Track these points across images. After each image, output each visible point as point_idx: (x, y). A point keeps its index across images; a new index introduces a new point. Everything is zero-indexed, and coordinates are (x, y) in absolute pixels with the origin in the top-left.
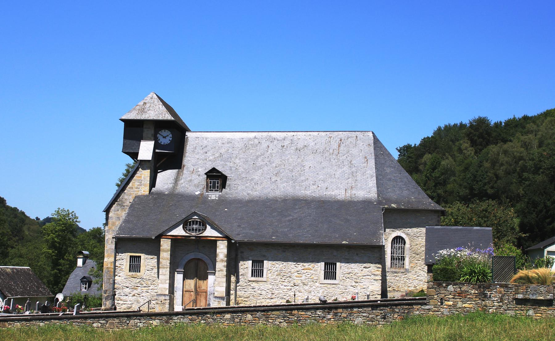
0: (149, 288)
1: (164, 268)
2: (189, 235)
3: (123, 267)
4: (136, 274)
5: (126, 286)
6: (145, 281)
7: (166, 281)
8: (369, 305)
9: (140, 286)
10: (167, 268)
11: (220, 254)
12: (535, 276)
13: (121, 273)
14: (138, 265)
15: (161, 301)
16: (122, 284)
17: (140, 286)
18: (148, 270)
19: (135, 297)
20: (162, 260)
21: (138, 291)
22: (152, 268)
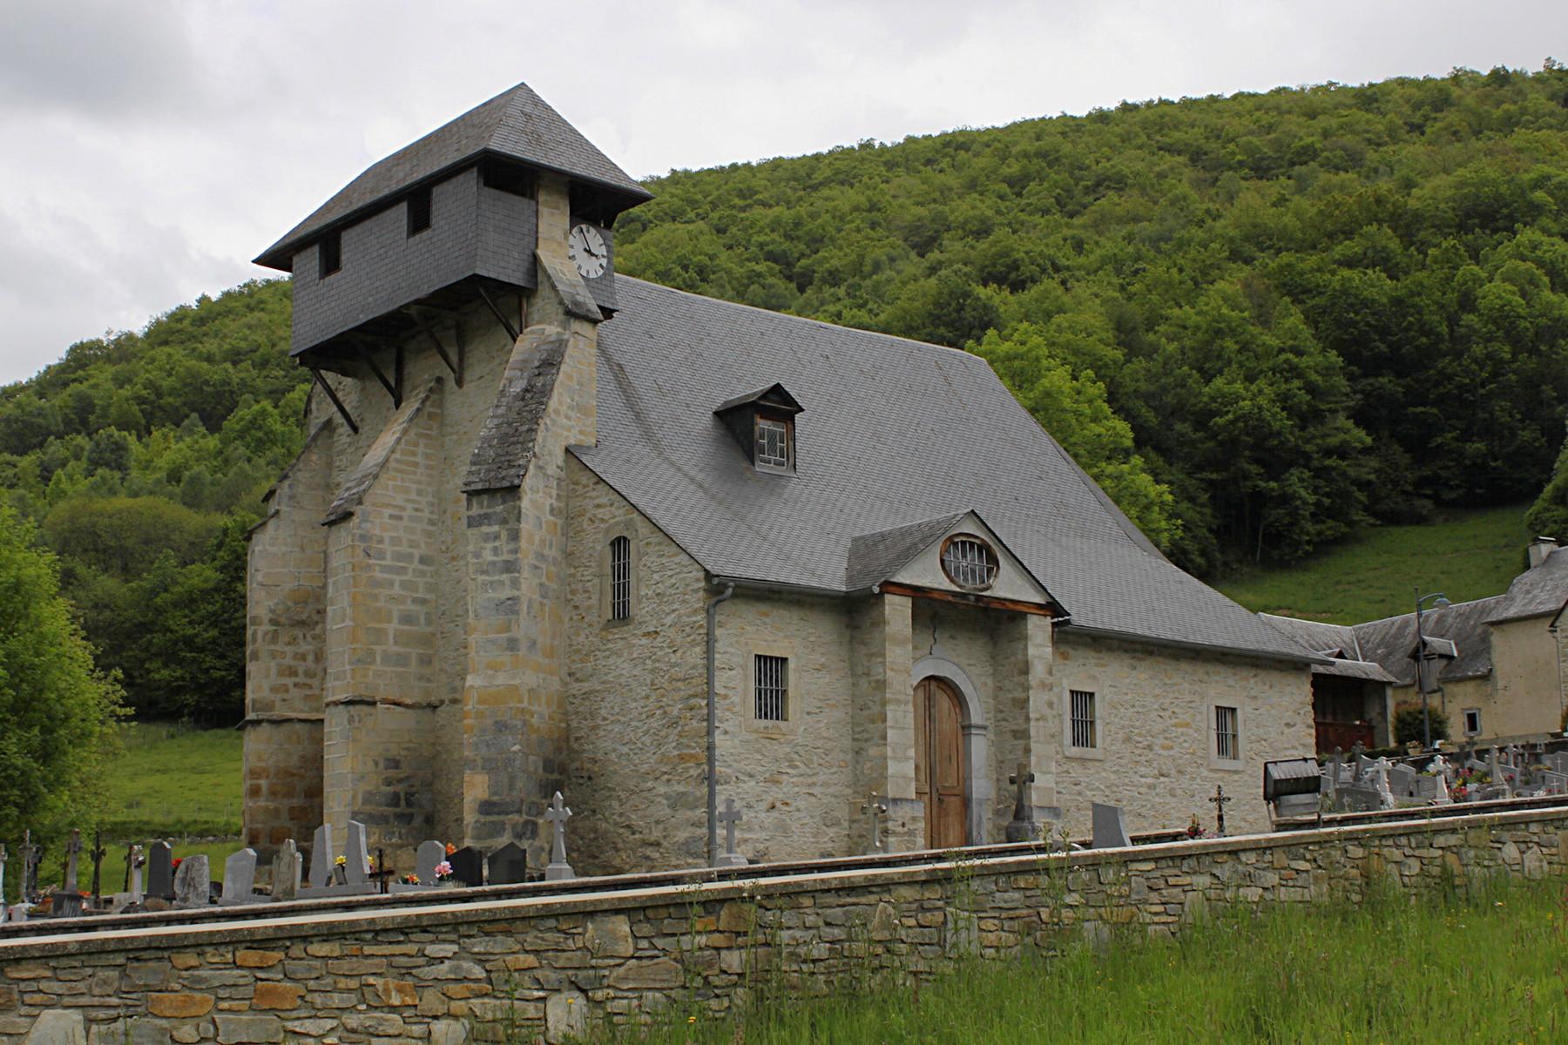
0: (814, 779)
1: (898, 702)
2: (958, 590)
3: (736, 699)
4: (778, 727)
5: (749, 769)
6: (803, 753)
7: (906, 750)
8: (271, 934)
9: (789, 771)
10: (906, 703)
11: (1036, 661)
12: (979, 823)
13: (730, 723)
14: (766, 691)
15: (903, 825)
16: (735, 765)
17: (789, 771)
18: (808, 713)
19: (775, 814)
20: (892, 674)
21: (785, 790)
22: (819, 704)
